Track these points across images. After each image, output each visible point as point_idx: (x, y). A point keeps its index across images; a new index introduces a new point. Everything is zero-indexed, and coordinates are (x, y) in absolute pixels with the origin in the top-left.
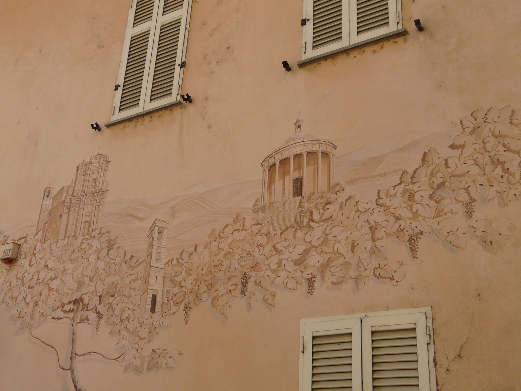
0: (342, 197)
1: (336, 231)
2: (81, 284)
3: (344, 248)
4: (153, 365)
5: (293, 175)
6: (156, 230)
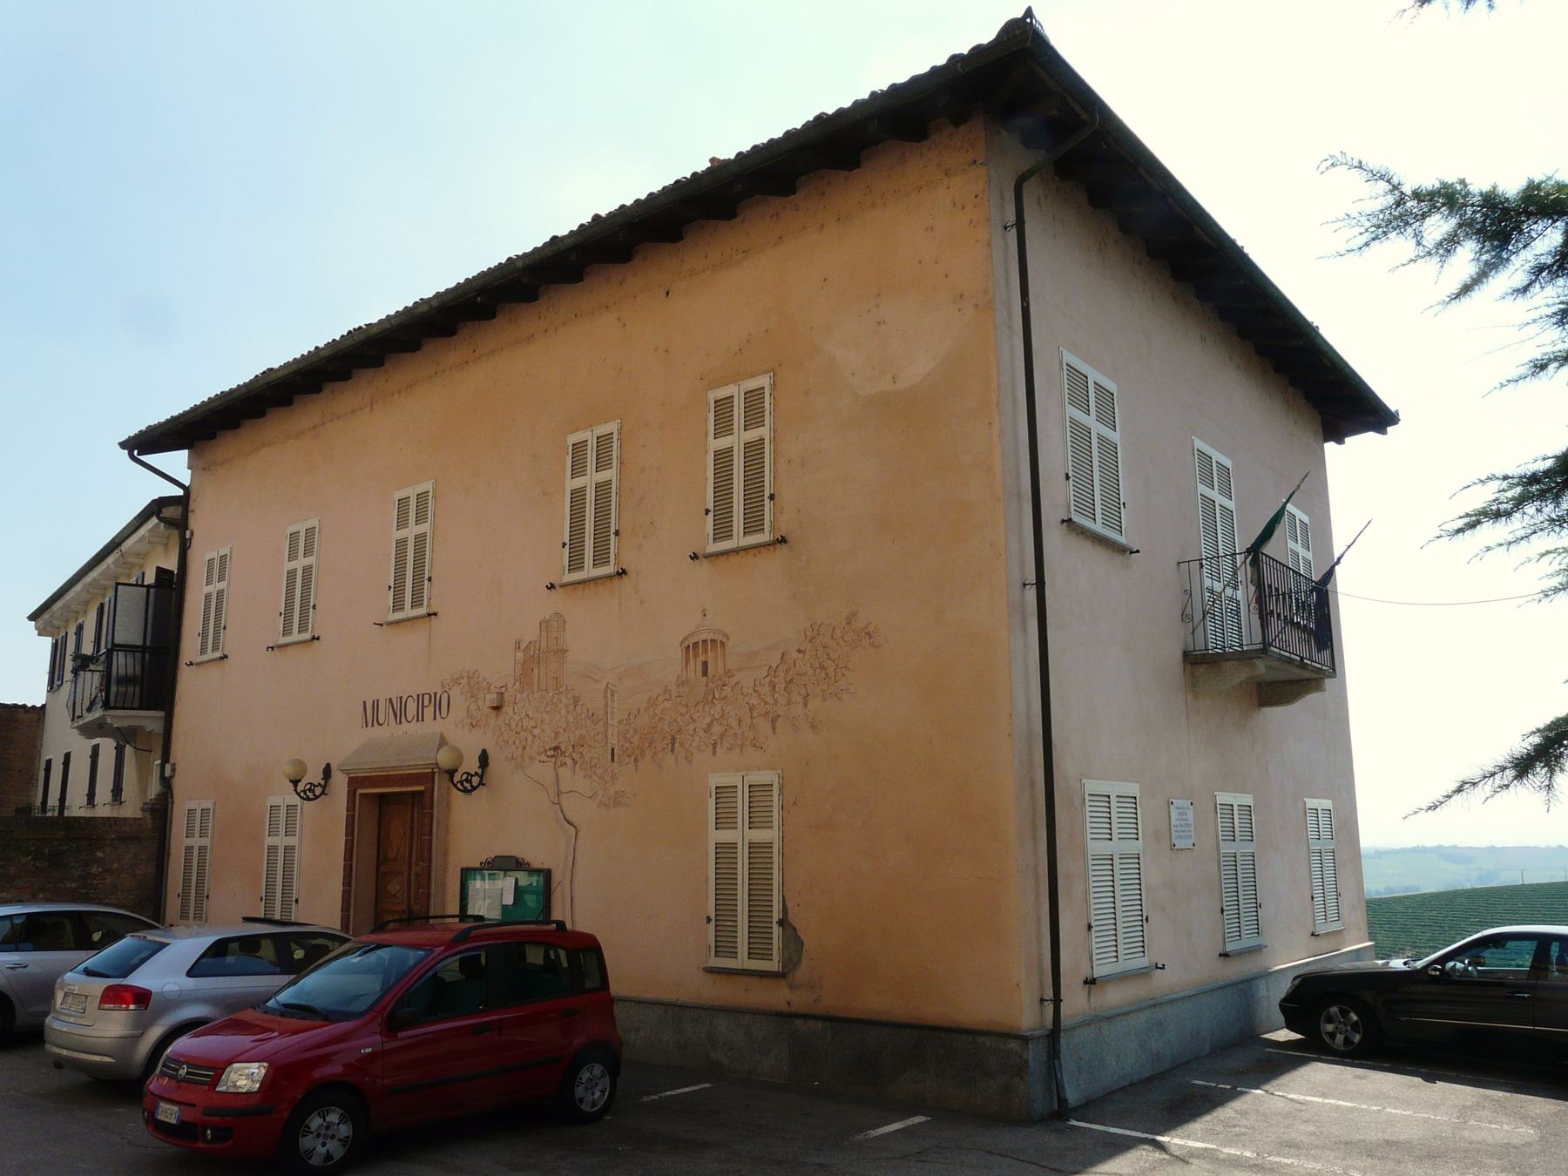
0: (733, 681)
1: (729, 708)
2: (557, 734)
3: (734, 723)
4: (617, 803)
5: (702, 658)
6: (609, 692)
